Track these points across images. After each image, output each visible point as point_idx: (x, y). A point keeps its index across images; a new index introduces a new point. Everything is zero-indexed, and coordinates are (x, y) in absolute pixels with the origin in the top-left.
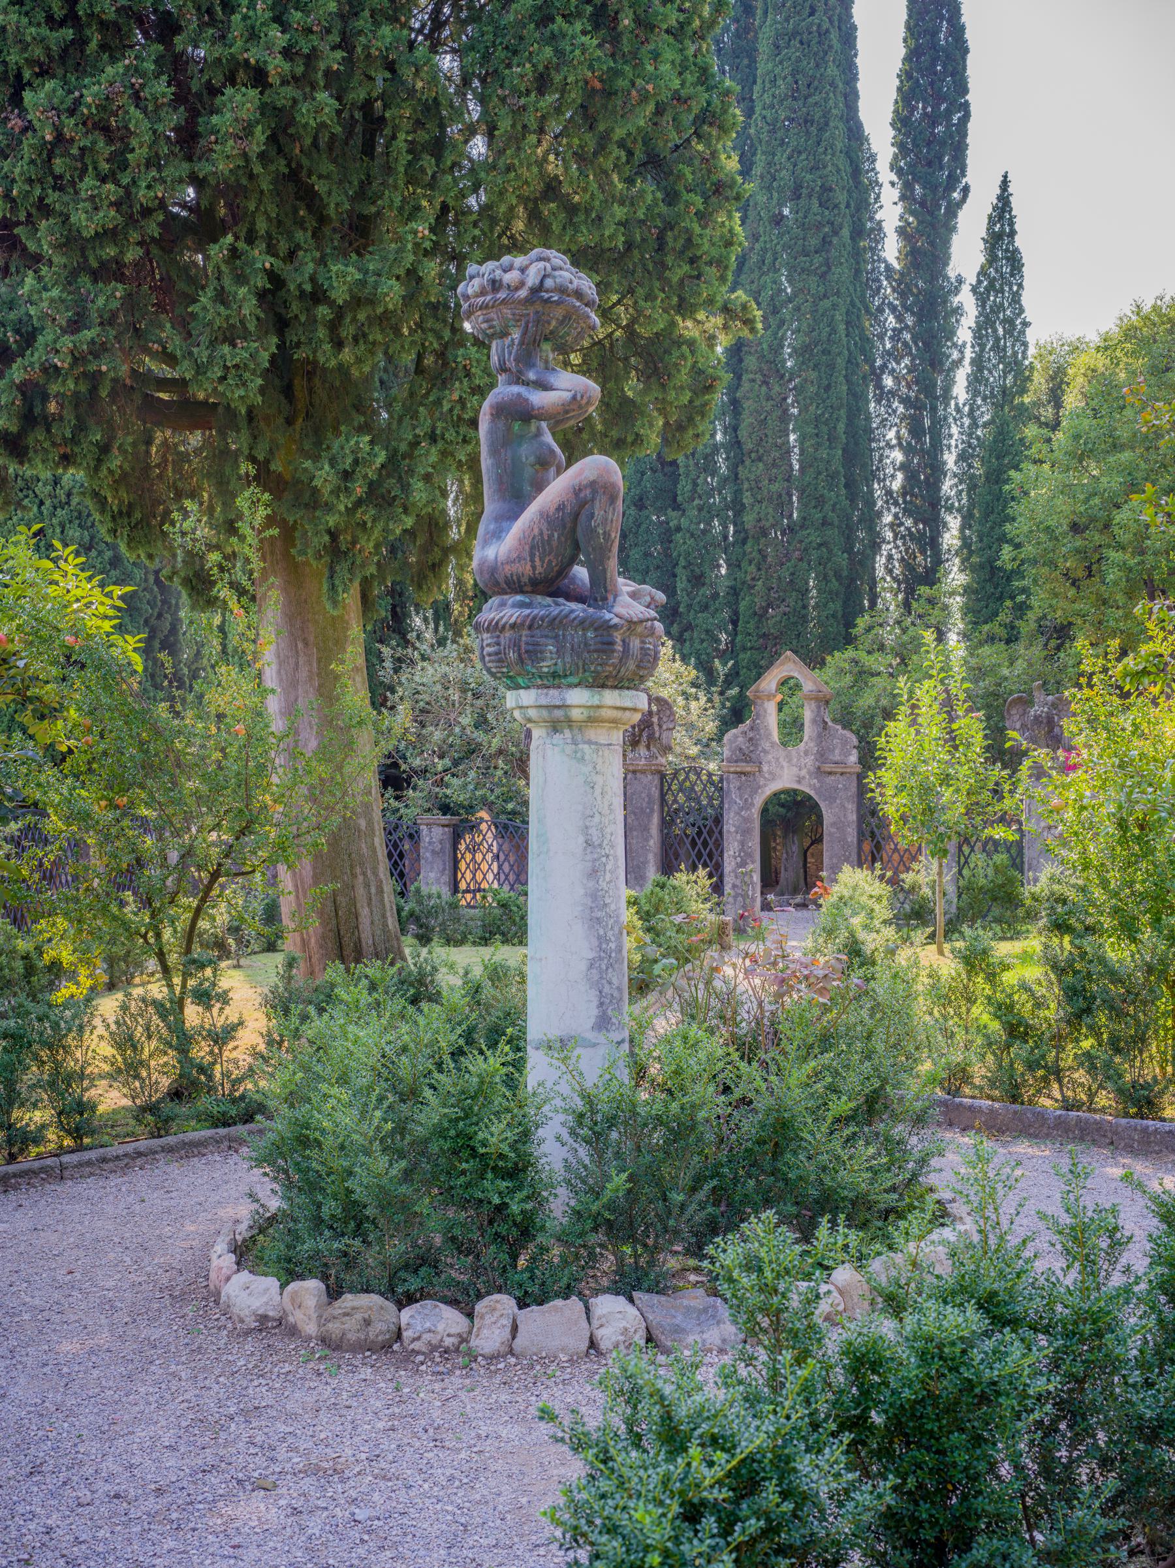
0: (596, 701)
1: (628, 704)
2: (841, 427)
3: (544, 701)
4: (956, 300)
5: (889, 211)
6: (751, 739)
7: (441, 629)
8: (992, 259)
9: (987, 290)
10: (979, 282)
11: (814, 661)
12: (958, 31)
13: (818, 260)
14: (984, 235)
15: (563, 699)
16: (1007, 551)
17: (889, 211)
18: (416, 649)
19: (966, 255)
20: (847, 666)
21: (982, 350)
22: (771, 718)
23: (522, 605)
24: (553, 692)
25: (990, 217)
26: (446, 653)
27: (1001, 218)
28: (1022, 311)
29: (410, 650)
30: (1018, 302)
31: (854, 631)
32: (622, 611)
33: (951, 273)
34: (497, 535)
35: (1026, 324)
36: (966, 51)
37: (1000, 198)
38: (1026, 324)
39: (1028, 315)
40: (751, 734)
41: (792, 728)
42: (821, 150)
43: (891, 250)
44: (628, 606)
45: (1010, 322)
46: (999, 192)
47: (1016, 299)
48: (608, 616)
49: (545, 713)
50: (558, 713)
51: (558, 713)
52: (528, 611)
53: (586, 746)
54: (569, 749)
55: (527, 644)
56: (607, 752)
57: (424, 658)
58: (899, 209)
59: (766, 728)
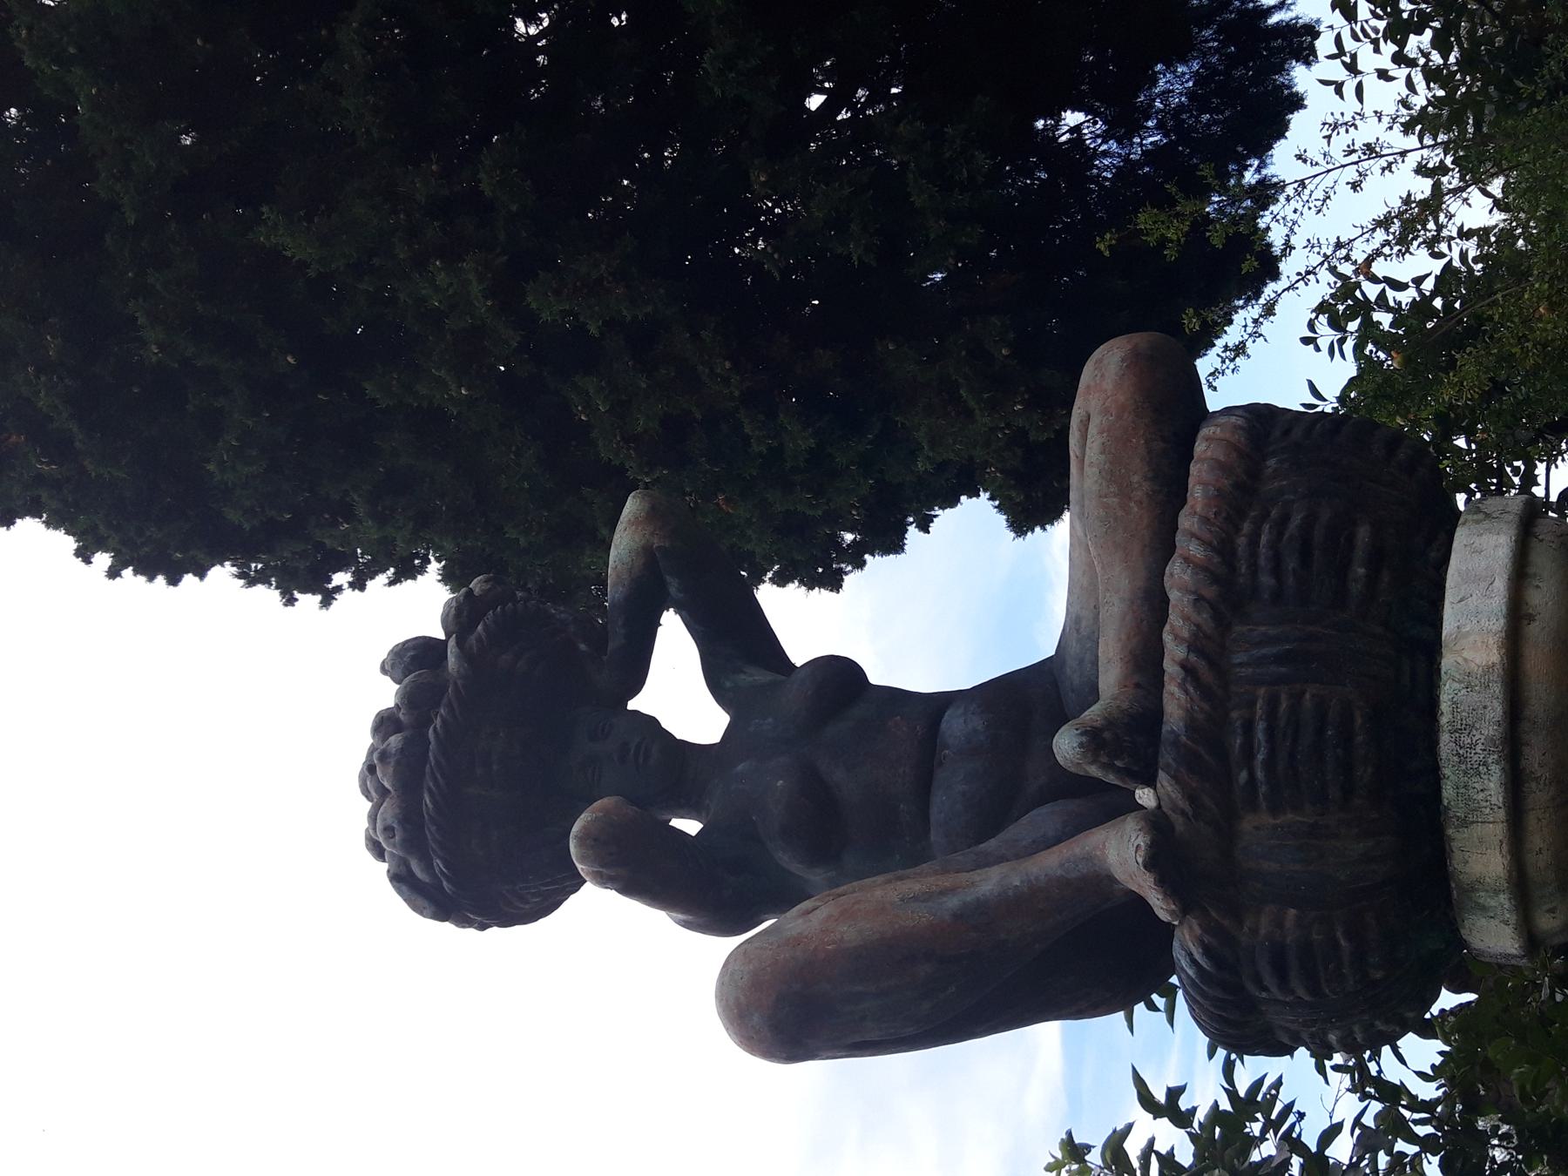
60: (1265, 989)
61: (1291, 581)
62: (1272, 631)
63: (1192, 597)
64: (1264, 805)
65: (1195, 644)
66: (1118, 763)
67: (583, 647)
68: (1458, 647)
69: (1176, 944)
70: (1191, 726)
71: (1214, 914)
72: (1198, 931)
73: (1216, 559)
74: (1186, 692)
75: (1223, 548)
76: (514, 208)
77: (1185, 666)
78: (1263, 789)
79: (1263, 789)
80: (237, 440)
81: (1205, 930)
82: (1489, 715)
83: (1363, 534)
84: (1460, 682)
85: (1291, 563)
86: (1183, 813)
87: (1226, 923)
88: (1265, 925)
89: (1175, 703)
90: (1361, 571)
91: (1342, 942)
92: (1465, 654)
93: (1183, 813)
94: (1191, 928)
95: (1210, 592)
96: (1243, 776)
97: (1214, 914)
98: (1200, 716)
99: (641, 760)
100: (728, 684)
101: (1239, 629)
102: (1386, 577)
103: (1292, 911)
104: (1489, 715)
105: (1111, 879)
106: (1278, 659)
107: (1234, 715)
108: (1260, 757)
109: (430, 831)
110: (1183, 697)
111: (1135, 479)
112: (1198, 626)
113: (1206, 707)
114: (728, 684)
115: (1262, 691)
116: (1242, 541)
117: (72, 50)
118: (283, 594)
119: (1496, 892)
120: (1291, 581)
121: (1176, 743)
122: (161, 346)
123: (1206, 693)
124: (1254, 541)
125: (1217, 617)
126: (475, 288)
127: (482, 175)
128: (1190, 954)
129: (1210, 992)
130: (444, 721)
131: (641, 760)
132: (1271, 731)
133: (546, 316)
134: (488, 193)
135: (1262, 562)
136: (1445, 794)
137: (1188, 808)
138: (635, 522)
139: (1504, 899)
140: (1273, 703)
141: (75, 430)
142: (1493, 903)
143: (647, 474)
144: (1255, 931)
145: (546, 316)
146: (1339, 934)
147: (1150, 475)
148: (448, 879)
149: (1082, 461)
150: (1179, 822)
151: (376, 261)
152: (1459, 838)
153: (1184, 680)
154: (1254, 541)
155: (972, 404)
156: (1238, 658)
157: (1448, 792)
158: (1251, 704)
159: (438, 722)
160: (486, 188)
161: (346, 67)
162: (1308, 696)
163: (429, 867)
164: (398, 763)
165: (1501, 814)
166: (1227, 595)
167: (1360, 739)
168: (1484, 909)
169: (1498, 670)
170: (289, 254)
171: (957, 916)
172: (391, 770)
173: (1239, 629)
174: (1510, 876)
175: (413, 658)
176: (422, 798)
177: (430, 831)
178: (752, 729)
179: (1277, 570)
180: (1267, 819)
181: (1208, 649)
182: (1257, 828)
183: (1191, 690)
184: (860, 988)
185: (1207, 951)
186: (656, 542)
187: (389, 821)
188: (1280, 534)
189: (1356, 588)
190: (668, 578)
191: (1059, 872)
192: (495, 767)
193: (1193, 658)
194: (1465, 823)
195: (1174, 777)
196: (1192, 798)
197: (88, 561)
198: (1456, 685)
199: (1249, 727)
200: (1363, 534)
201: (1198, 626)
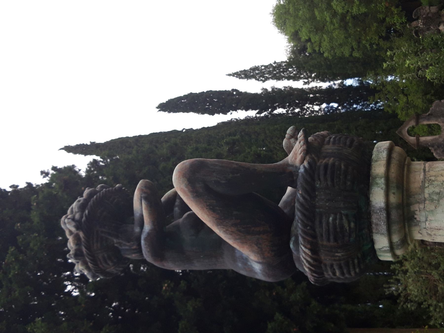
0: (381, 182)
1: (384, 155)
2: (311, 125)
3: (383, 227)
4: (270, 90)
5: (241, 115)
6: (438, 147)
7: (392, 281)
8: (254, 77)
9: (264, 77)
10: (261, 80)
11: (401, 124)
12: (185, 97)
13: (253, 136)
14: (246, 80)
15: (380, 209)
16: (356, 54)
17: (241, 115)
18: (402, 292)
19: (254, 87)
20: (404, 113)
21: (284, 77)
22: (426, 139)
23: (297, 243)
24: (374, 219)
25: (240, 78)
26: (403, 279)
27: (240, 75)
28: (271, 65)
29: (402, 294)
30: (267, 66)
31: (390, 112)
32: (299, 157)
33: (259, 91)
34: (245, 261)
35: (275, 63)
36: (191, 93)
37: (233, 76)
38: (275, 63)
39: (272, 62)
40: (436, 147)
41: (432, 130)
42: (218, 137)
43: (252, 113)
44: (295, 154)
45: (274, 68)
46: (231, 77)
47: (266, 67)
48: (302, 170)
49: (395, 228)
50: (394, 215)
51: (394, 215)
52: (300, 239)
53: (427, 191)
54: (429, 206)
55: (329, 240)
56: (432, 173)
57: (405, 289)
58: (239, 111)
59: (432, 140)
87: (316, 158)
157: (374, 156)
165: (385, 159)
194: (376, 161)
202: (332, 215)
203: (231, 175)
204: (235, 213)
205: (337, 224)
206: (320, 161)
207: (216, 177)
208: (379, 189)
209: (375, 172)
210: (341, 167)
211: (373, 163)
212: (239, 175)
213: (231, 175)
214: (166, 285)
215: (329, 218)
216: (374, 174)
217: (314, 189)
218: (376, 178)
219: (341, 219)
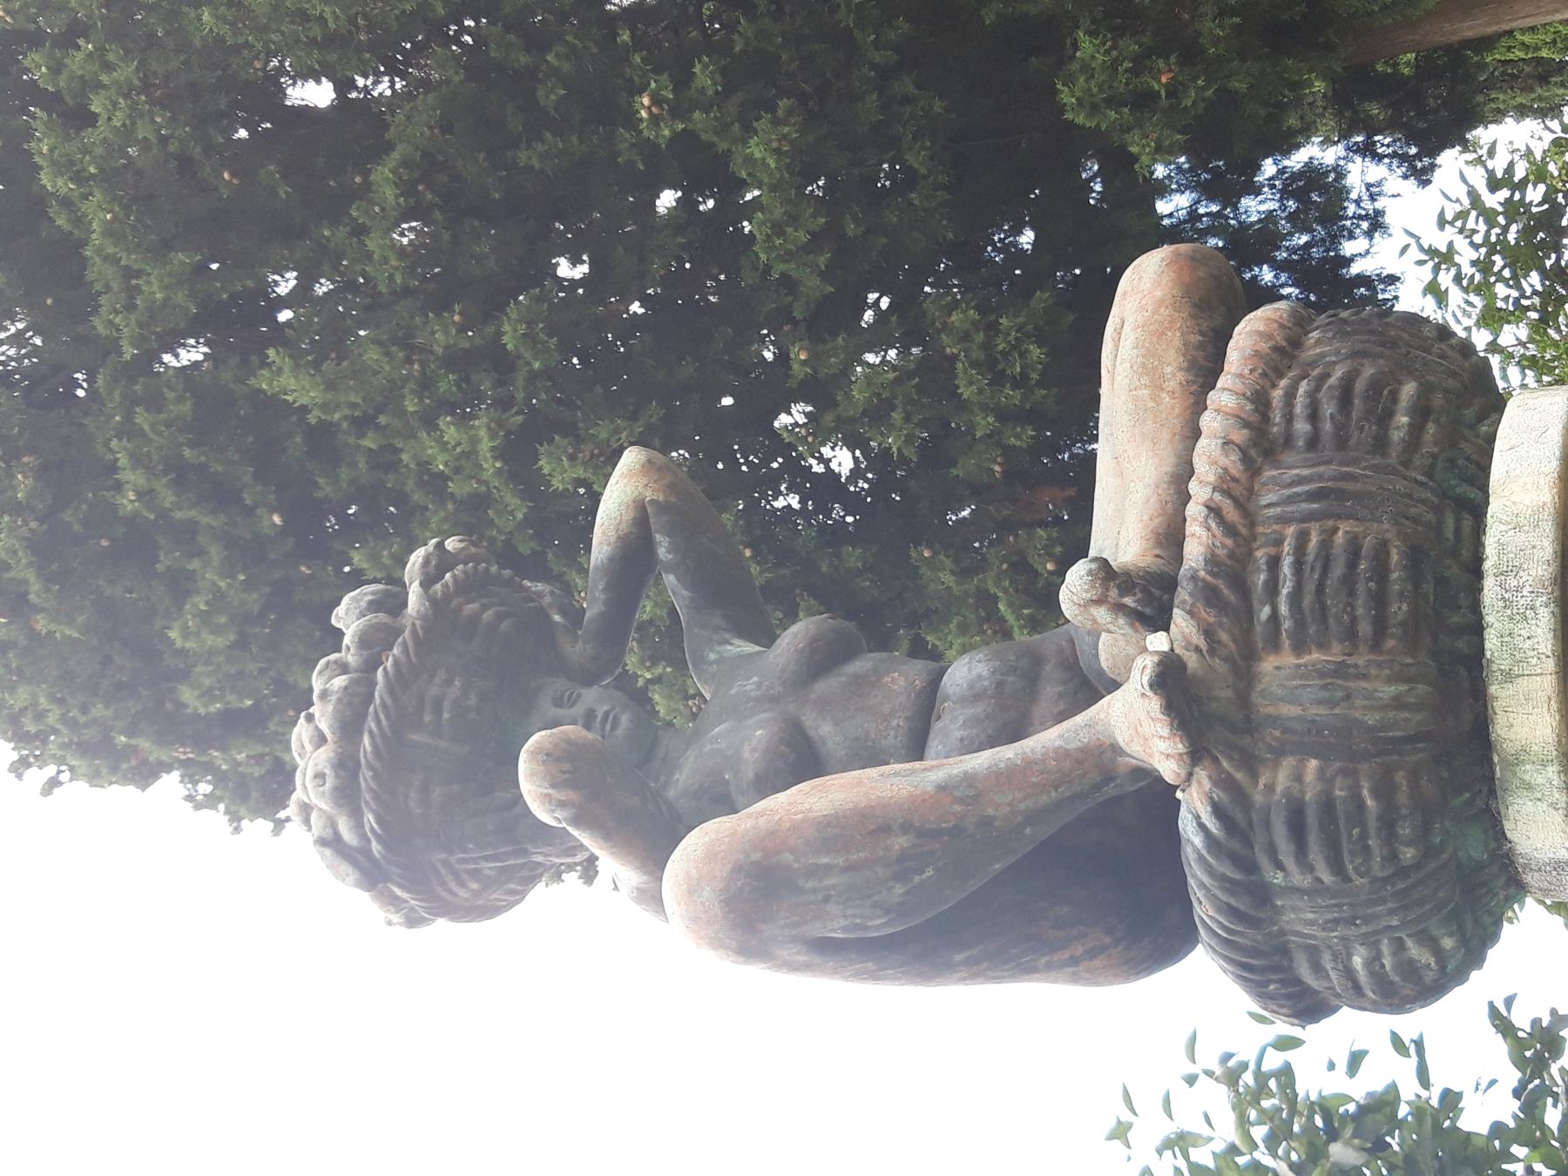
60: (1280, 866)
61: (1327, 426)
62: (1306, 472)
63: (1220, 441)
64: (1287, 643)
65: (1225, 485)
66: (1128, 601)
67: (557, 618)
68: (1506, 492)
69: (1191, 881)
70: (1212, 561)
71: (1225, 764)
72: (1207, 785)
73: (1249, 407)
74: (1209, 529)
75: (1260, 400)
76: (537, 365)
77: (1213, 510)
78: (1287, 625)
79: (1287, 625)
80: (207, 603)
81: (1216, 783)
82: (1538, 554)
83: (1408, 390)
84: (1508, 523)
85: (1328, 409)
86: (1198, 650)
87: (1239, 776)
88: (1282, 779)
89: (1198, 543)
90: (1405, 420)
91: (1369, 802)
92: (1514, 498)
93: (1198, 650)
94: (1199, 783)
95: (1240, 436)
96: (1266, 612)
97: (1225, 764)
98: (1222, 552)
99: (608, 727)
100: (712, 656)
101: (1269, 473)
102: (1431, 428)
103: (1313, 763)
104: (1538, 554)
105: (1116, 749)
106: (1313, 496)
107: (1259, 554)
108: (1285, 591)
109: (365, 777)
110: (1204, 533)
111: (1168, 370)
112: (1225, 469)
113: (1229, 542)
114: (712, 656)
115: (1291, 530)
116: (1277, 394)
117: (92, 170)
118: (231, 821)
119: (1544, 764)
120: (1327, 426)
121: (1194, 578)
122: (140, 495)
123: (1229, 529)
124: (1290, 394)
125: (1246, 459)
126: (485, 445)
127: (507, 327)
128: (1198, 818)
129: (1219, 894)
130: (396, 663)
131: (608, 727)
132: (1298, 566)
133: (557, 484)
134: (510, 347)
135: (1298, 410)
136: (1488, 645)
137: (1203, 645)
138: (630, 474)
139: (1552, 772)
140: (1302, 538)
141: (32, 579)
142: (1540, 780)
143: (648, 669)
144: (1270, 788)
145: (557, 484)
146: (1365, 792)
147: (1185, 365)
148: (379, 838)
149: (1112, 374)
150: (1192, 661)
151: (382, 419)
152: (1502, 695)
153: (1207, 517)
154: (1290, 394)
155: (1011, 618)
156: (1265, 501)
157: (1491, 643)
158: (1279, 542)
159: (389, 664)
160: (509, 341)
161: (377, 209)
162: (1340, 533)
163: (359, 824)
164: (339, 700)
165: (1550, 665)
166: (1261, 442)
167: (1395, 575)
168: (1529, 787)
169: (1550, 509)
170: (289, 398)
171: (942, 788)
172: (330, 708)
173: (1269, 473)
174: (1559, 742)
175: (370, 603)
176: (361, 741)
177: (365, 777)
178: (733, 692)
179: (1314, 416)
180: (1288, 659)
181: (1238, 493)
182: (1278, 668)
183: (1213, 525)
184: (826, 860)
185: (1218, 810)
186: (649, 495)
187: (320, 767)
188: (1318, 389)
189: (1397, 436)
190: (658, 537)
191: (1058, 743)
192: (446, 715)
193: (1217, 497)
194: (1509, 677)
195: (1191, 613)
196: (1208, 633)
197: (19, 777)
198: (1504, 528)
199: (1274, 563)
200: (1408, 390)
201: (1225, 469)
202: (1362, 950)
203: (899, 889)
204: (958, 958)
205: (1388, 967)
206: (1262, 782)
207: (845, 917)
208: (1543, 806)
209: (1511, 736)
210: (1361, 805)
211: (1493, 689)
212: (929, 872)
213: (899, 889)
214: (646, 101)
215: (1349, 956)
216: (1509, 748)
217: (1262, 894)
218: (1518, 762)
219: (1399, 946)
